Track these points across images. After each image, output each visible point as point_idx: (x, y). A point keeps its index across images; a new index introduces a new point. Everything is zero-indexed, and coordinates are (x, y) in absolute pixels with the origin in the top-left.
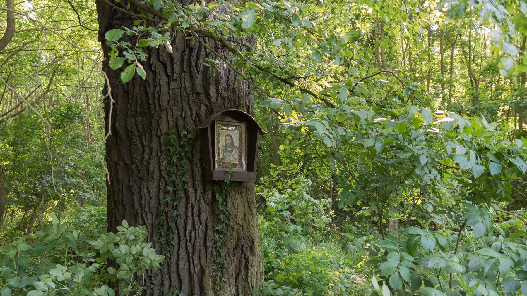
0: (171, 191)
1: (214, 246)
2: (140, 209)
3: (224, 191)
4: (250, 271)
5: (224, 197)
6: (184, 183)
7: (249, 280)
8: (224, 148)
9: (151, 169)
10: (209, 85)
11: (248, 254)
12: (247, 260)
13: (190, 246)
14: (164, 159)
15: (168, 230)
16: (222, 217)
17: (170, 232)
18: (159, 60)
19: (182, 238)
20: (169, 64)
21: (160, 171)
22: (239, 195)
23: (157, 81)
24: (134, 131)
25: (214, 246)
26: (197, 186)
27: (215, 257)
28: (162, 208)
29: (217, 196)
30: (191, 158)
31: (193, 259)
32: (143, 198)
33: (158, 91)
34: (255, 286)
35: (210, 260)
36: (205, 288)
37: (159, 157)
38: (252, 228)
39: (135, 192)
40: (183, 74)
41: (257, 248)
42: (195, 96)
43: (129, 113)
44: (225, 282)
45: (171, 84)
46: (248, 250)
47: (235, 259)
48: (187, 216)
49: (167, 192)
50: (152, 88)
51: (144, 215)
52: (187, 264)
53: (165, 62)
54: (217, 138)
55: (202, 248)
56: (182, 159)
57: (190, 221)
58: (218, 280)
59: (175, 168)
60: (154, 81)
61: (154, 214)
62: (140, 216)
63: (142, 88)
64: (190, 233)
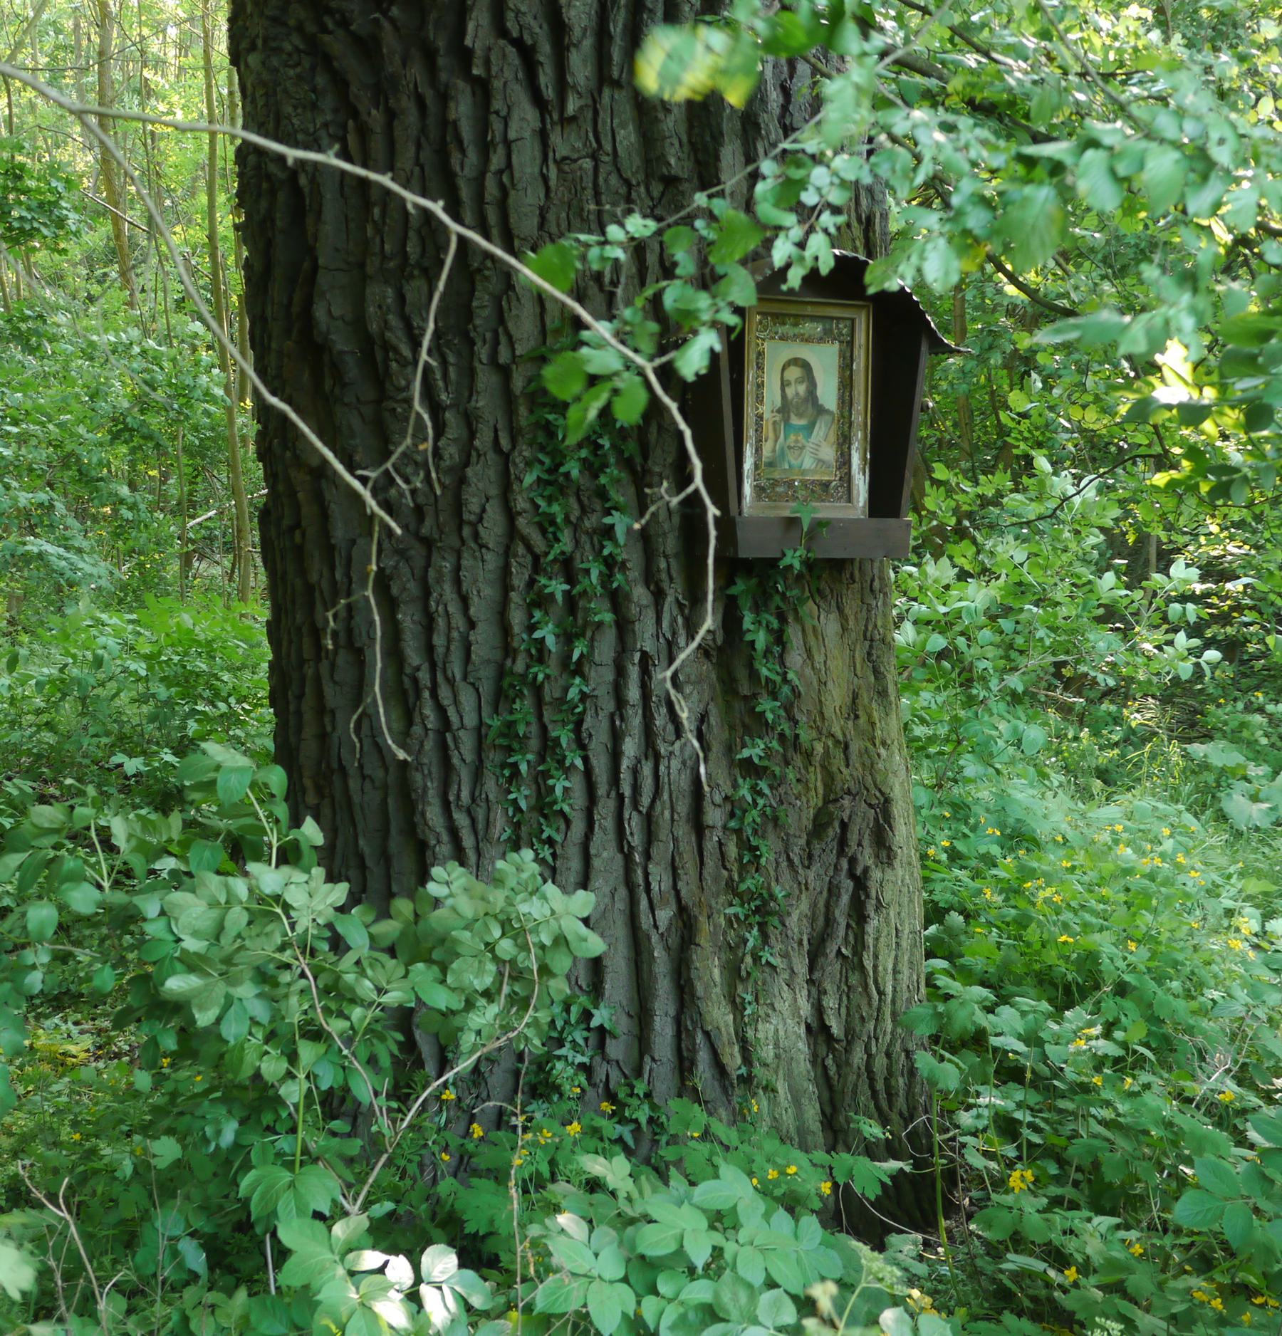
0: (559, 597)
1: (732, 824)
2: (425, 667)
3: (777, 599)
4: (870, 928)
5: (775, 624)
6: (610, 564)
7: (868, 964)
8: (778, 417)
9: (473, 504)
10: (718, 138)
11: (866, 857)
12: (860, 882)
13: (634, 824)
14: (529, 464)
15: (542, 759)
16: (767, 706)
17: (550, 763)
18: (502, 32)
19: (602, 790)
20: (545, 51)
21: (511, 515)
22: (834, 616)
23: (497, 125)
24: (394, 341)
25: (732, 824)
26: (664, 576)
27: (735, 868)
28: (519, 667)
29: (748, 620)
30: (638, 460)
31: (646, 875)
32: (441, 622)
33: (500, 172)
34: (889, 990)
35: (716, 879)
36: (700, 989)
37: (505, 458)
38: (882, 751)
39: (405, 596)
40: (607, 92)
41: (904, 833)
42: (657, 189)
43: (372, 265)
44: (774, 968)
45: (555, 138)
46: (866, 842)
47: (811, 875)
48: (621, 702)
49: (541, 601)
50: (472, 156)
51: (444, 693)
52: (622, 892)
53: (528, 40)
54: (750, 375)
55: (683, 831)
56: (605, 465)
57: (635, 721)
58: (749, 959)
59: (573, 501)
60: (483, 127)
61: (486, 688)
62: (426, 694)
63: (427, 155)
64: (635, 772)
